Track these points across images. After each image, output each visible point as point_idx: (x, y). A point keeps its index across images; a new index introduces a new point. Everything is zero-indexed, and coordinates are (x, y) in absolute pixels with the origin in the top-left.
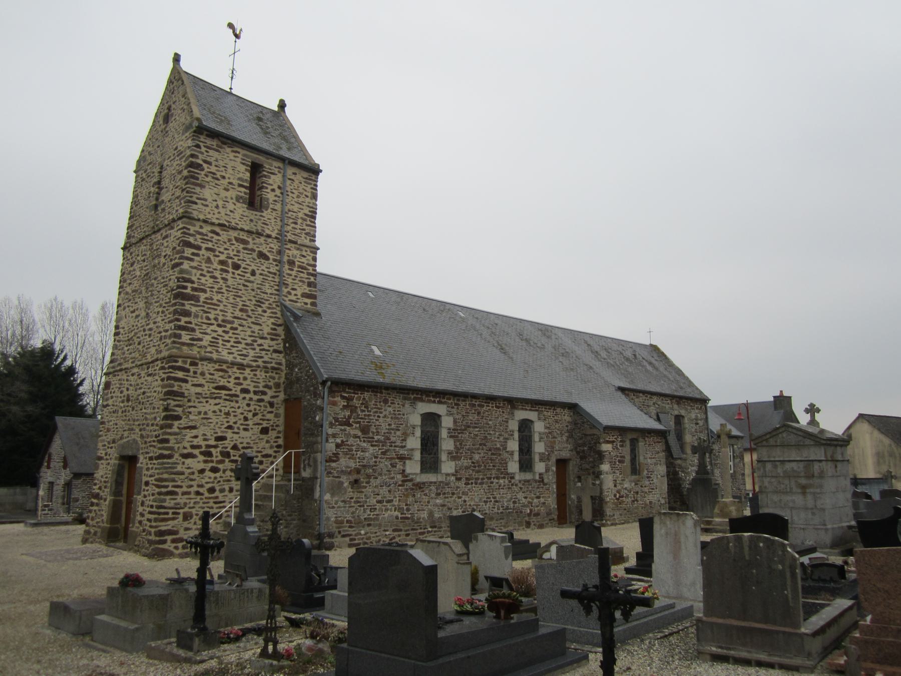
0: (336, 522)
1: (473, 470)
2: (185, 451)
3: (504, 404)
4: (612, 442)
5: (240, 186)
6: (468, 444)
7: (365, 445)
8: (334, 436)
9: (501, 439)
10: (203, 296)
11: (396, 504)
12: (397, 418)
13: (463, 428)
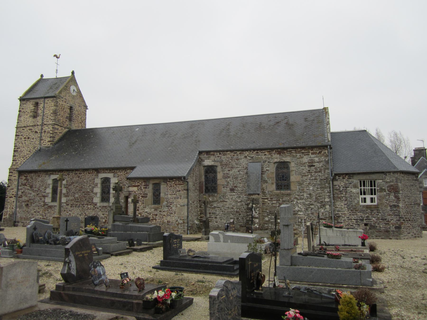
0: (21, 218)
1: (75, 201)
2: (10, 196)
3: (92, 172)
4: (138, 186)
5: (31, 112)
6: (72, 190)
7: (31, 192)
8: (21, 189)
9: (91, 187)
10: (19, 150)
11: (41, 213)
12: (43, 182)
13: (71, 183)
